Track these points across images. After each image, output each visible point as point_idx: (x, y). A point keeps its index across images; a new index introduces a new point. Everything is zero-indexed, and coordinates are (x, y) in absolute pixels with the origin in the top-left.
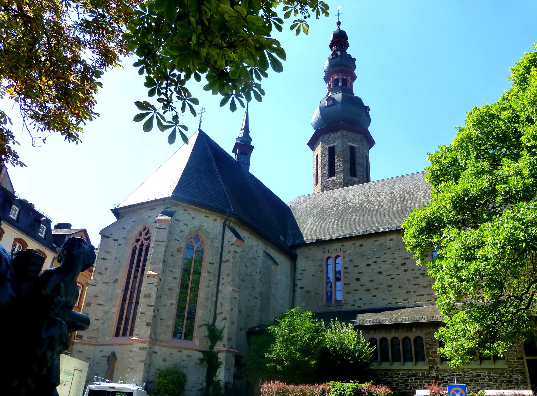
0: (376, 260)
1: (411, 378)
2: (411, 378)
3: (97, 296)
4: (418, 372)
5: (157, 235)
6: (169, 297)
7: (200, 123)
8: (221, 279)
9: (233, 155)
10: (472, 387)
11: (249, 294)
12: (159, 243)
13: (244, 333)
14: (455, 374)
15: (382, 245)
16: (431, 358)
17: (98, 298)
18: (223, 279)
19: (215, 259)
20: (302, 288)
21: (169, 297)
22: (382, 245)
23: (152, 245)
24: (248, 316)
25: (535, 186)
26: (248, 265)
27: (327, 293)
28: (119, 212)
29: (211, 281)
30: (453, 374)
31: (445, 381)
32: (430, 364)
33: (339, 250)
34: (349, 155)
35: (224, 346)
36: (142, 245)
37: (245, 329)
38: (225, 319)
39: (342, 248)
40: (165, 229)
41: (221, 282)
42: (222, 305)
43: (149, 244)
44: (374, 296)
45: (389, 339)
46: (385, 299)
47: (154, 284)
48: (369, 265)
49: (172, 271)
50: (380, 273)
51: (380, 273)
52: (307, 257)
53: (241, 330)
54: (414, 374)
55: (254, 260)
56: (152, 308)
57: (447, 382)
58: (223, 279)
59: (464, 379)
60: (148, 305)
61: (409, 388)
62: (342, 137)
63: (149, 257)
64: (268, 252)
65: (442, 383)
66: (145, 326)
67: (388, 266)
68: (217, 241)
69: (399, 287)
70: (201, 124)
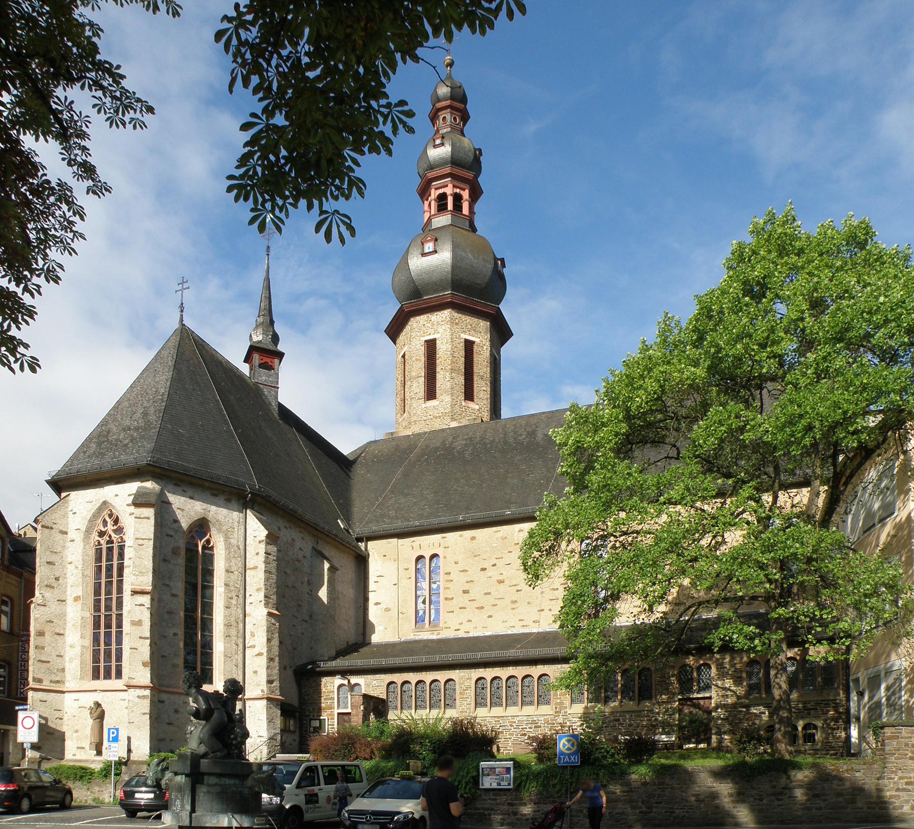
0: (495, 561)
1: (530, 726)
2: (530, 726)
3: (51, 622)
4: (540, 719)
5: (136, 530)
6: (170, 625)
7: (182, 311)
8: (247, 595)
9: (245, 369)
11: (294, 616)
12: (141, 542)
13: (290, 672)
15: (506, 538)
16: (558, 701)
19: (237, 565)
20: (377, 604)
21: (170, 625)
22: (506, 538)
24: (294, 649)
26: (288, 571)
27: (417, 612)
28: (60, 484)
29: (231, 598)
32: (556, 708)
33: (436, 545)
34: (463, 359)
35: (263, 691)
37: (291, 667)
38: (260, 654)
39: (442, 541)
40: (148, 518)
41: (248, 601)
42: (253, 635)
43: (123, 540)
44: (490, 616)
45: (504, 678)
46: (506, 621)
47: (144, 605)
48: (483, 569)
49: (168, 586)
50: (501, 582)
51: (501, 582)
52: (385, 556)
53: (285, 668)
55: (296, 563)
56: (148, 641)
60: (140, 638)
62: (452, 322)
63: (126, 562)
64: (319, 549)
67: (513, 571)
69: (529, 603)
70: (184, 314)
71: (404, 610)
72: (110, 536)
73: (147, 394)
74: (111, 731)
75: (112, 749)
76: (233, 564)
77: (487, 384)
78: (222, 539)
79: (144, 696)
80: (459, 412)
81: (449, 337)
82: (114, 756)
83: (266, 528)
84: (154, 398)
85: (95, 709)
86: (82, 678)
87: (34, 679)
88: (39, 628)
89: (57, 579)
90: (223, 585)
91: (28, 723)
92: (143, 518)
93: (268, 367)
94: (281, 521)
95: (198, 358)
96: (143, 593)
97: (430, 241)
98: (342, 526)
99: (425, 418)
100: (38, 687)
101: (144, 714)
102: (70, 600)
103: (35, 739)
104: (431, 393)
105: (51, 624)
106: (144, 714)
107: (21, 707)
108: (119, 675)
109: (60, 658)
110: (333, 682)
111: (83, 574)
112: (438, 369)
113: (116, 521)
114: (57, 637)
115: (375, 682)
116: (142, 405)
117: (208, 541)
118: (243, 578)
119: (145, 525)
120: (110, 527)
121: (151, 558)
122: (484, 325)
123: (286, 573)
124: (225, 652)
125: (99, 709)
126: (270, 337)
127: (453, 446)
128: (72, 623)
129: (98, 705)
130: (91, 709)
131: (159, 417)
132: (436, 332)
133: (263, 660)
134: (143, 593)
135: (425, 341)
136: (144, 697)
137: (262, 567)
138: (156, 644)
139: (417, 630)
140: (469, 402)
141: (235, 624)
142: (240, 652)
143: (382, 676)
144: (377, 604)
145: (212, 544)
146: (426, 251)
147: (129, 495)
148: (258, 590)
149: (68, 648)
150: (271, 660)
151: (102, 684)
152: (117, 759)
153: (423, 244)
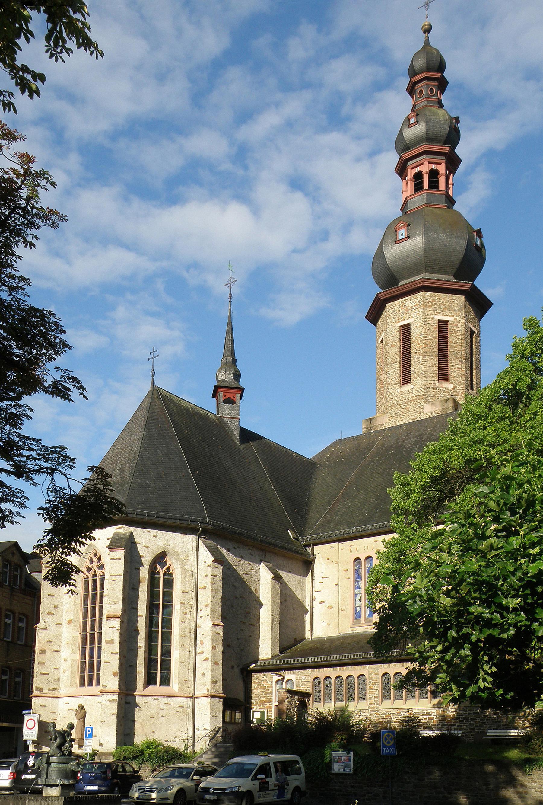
7: (153, 376)
10: (488, 726)
11: (241, 622)
12: (114, 578)
14: (472, 712)
17: (53, 643)
18: (201, 610)
19: (190, 586)
20: (322, 602)
23: (107, 577)
25: (542, 511)
27: (355, 608)
29: (186, 614)
30: (470, 712)
31: (461, 720)
34: (437, 340)
35: (208, 690)
36: (95, 575)
37: (238, 666)
38: (207, 659)
40: (120, 559)
41: (199, 615)
42: (202, 643)
43: (104, 575)
52: (328, 559)
54: (429, 713)
56: (118, 656)
57: (463, 721)
58: (201, 610)
59: (481, 718)
60: (112, 653)
61: (422, 729)
62: (425, 304)
65: (457, 722)
66: (112, 677)
68: (190, 562)
70: (155, 378)
71: (344, 608)
72: (95, 571)
73: (125, 452)
74: (88, 729)
75: (88, 744)
76: (187, 586)
77: (461, 361)
78: (179, 566)
79: (113, 700)
80: (433, 394)
81: (422, 321)
82: (89, 749)
83: (213, 555)
84: (129, 455)
85: (79, 711)
86: (71, 686)
87: (37, 688)
88: (41, 648)
89: (56, 607)
90: (179, 603)
91: (31, 724)
92: (116, 559)
93: (229, 401)
94: (230, 544)
95: (165, 415)
96: (115, 617)
97: (402, 227)
98: (291, 536)
99: (400, 402)
100: (39, 695)
101: (113, 714)
102: (65, 623)
103: (35, 737)
104: (406, 378)
105: (51, 644)
106: (113, 714)
107: (26, 712)
108: (98, 683)
109: (56, 670)
110: (272, 679)
111: (74, 602)
112: (412, 354)
113: (99, 559)
114: (55, 653)
115: (304, 678)
116: (120, 462)
117: (168, 569)
118: (195, 596)
119: (118, 565)
120: (95, 564)
121: (121, 590)
122: (459, 300)
123: (234, 586)
124: (179, 659)
125: (83, 711)
126: (232, 375)
127: (404, 444)
128: (66, 641)
129: (82, 707)
130: (77, 711)
131: (132, 473)
132: (410, 317)
133: (209, 664)
134: (115, 617)
135: (400, 326)
136: (113, 701)
137: (209, 586)
138: (124, 657)
139: (355, 625)
140: (443, 382)
141: (188, 635)
142: (192, 658)
143: (309, 672)
144: (322, 602)
145: (171, 571)
146: (400, 237)
147: (108, 539)
148: (207, 606)
149: (62, 662)
150: (216, 663)
151: (87, 689)
152: (91, 752)
153: (396, 231)
